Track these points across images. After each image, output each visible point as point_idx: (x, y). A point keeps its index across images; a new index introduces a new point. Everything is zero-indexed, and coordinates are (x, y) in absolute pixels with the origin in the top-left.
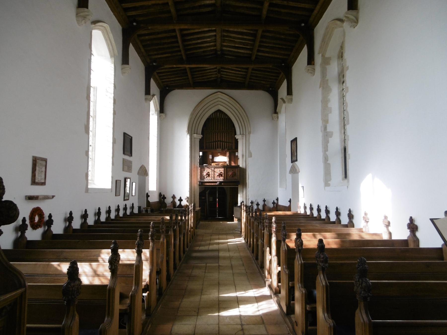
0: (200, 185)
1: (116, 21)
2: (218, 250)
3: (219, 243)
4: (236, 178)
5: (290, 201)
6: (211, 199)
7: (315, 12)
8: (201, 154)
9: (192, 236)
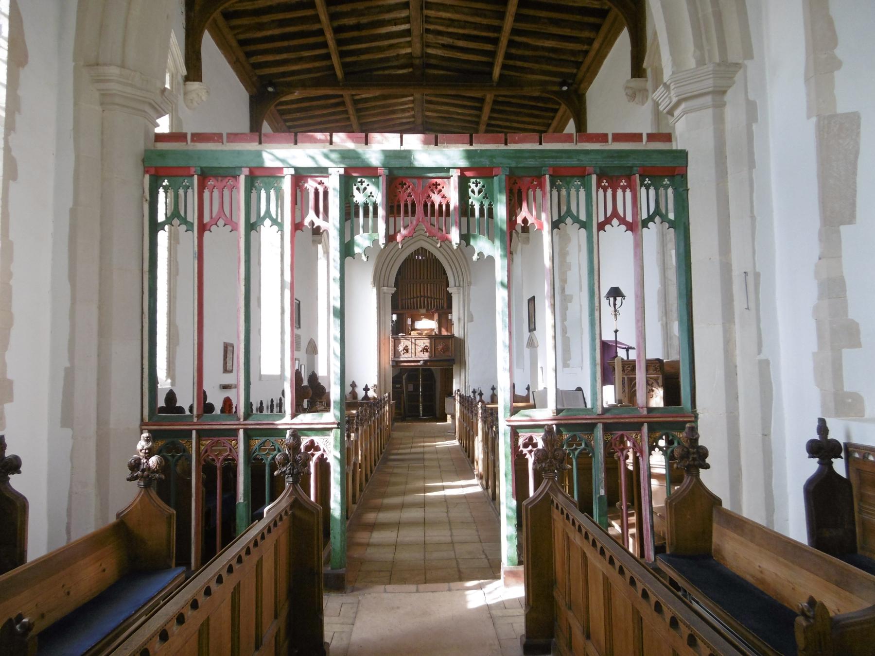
0: (393, 366)
1: (238, 80)
2: (423, 453)
3: (424, 446)
4: (448, 354)
5: (528, 389)
6: (411, 388)
7: (592, 53)
8: (395, 317)
9: (366, 476)
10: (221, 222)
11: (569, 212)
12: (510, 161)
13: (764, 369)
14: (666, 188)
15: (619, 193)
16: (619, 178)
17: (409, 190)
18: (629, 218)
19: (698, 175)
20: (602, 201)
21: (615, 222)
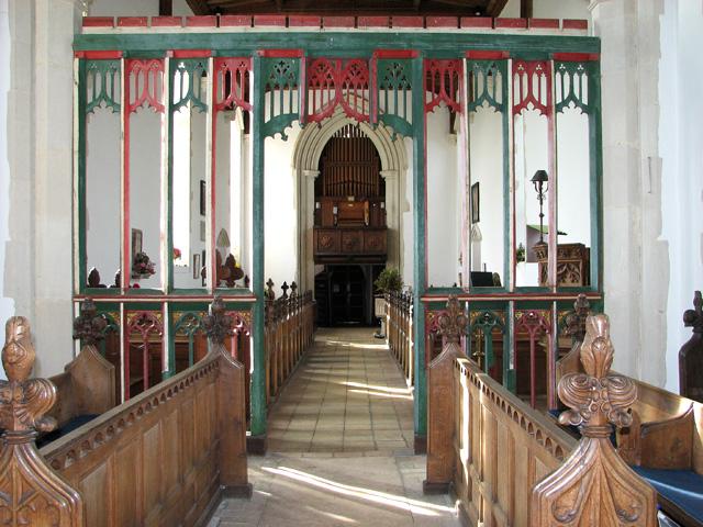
10: (146, 104)
11: (531, 98)
12: (427, 45)
14: (580, 74)
15: (576, 76)
16: (534, 63)
17: (329, 72)
19: (609, 62)
20: (516, 87)
21: (572, 104)
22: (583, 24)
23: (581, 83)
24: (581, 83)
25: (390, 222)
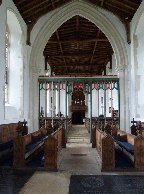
13: (129, 111)
18: (110, 88)
19: (121, 82)
22: (117, 75)
23: (116, 85)
24: (116, 85)
25: (86, 104)
